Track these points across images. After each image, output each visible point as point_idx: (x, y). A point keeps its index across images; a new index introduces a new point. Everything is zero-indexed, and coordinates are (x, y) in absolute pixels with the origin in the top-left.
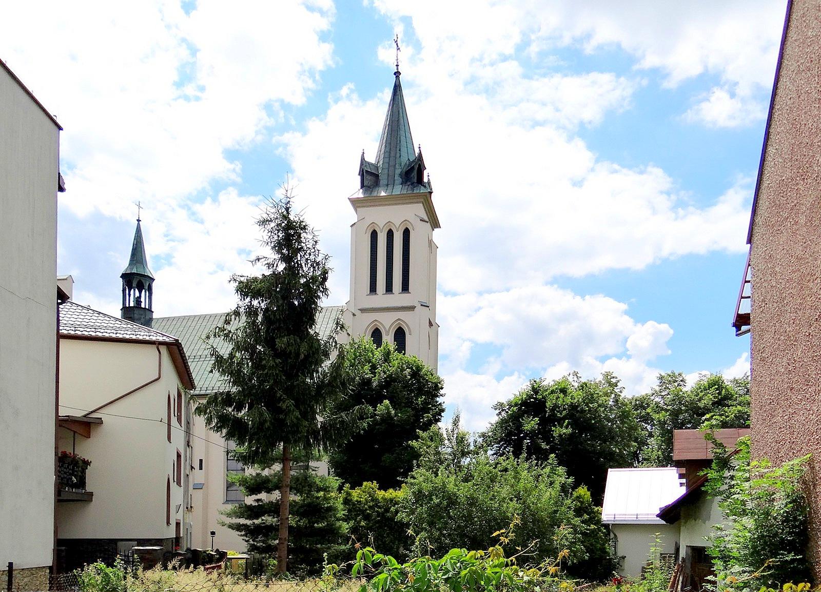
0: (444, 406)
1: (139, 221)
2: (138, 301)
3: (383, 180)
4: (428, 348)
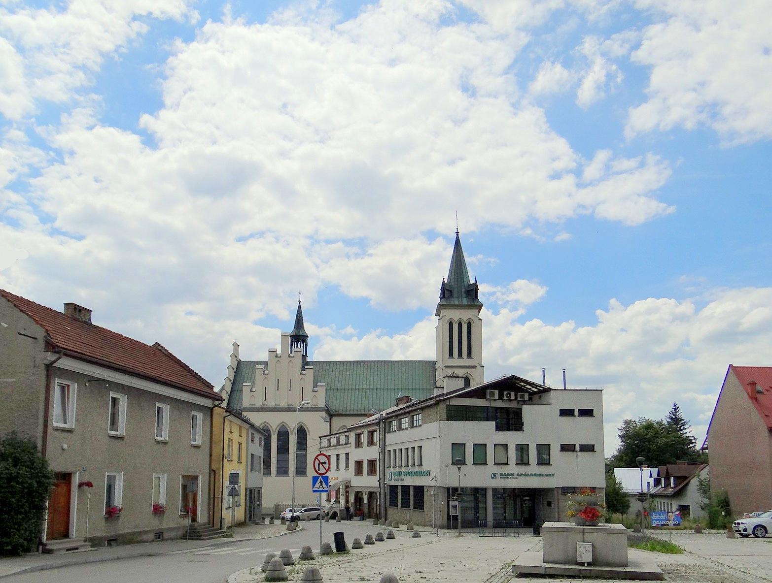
1: (300, 302)
3: (455, 294)
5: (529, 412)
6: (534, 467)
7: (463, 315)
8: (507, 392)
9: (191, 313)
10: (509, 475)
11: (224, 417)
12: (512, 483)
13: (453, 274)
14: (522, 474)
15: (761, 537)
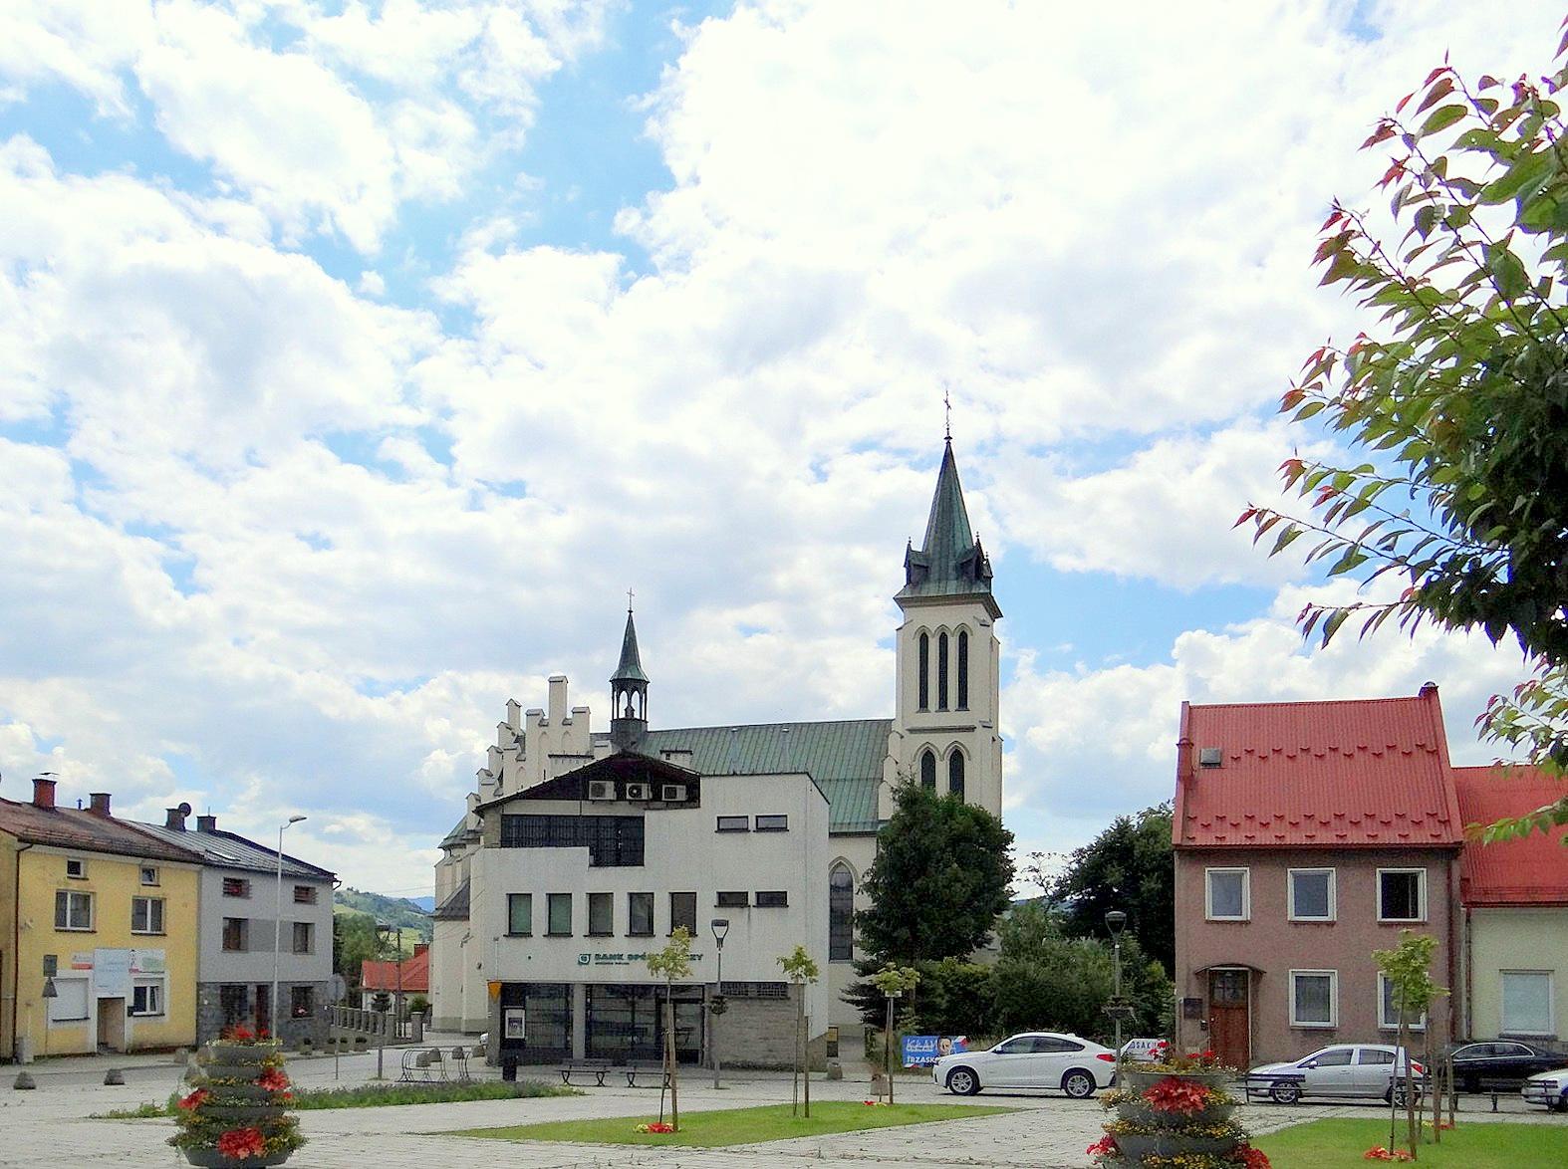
0: (1015, 864)
1: (630, 612)
2: (629, 710)
3: (934, 574)
4: (1411, 533)
5: (662, 827)
6: (659, 944)
7: (952, 617)
8: (630, 785)
9: (748, 631)
10: (612, 957)
11: (19, 852)
12: (620, 975)
13: (933, 532)
14: (637, 957)
15: (1081, 1098)
